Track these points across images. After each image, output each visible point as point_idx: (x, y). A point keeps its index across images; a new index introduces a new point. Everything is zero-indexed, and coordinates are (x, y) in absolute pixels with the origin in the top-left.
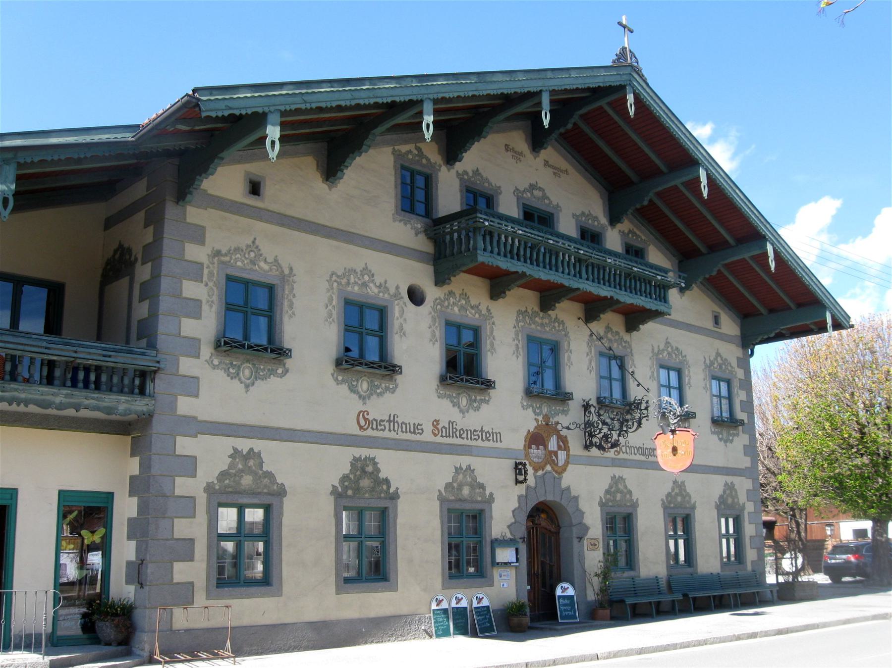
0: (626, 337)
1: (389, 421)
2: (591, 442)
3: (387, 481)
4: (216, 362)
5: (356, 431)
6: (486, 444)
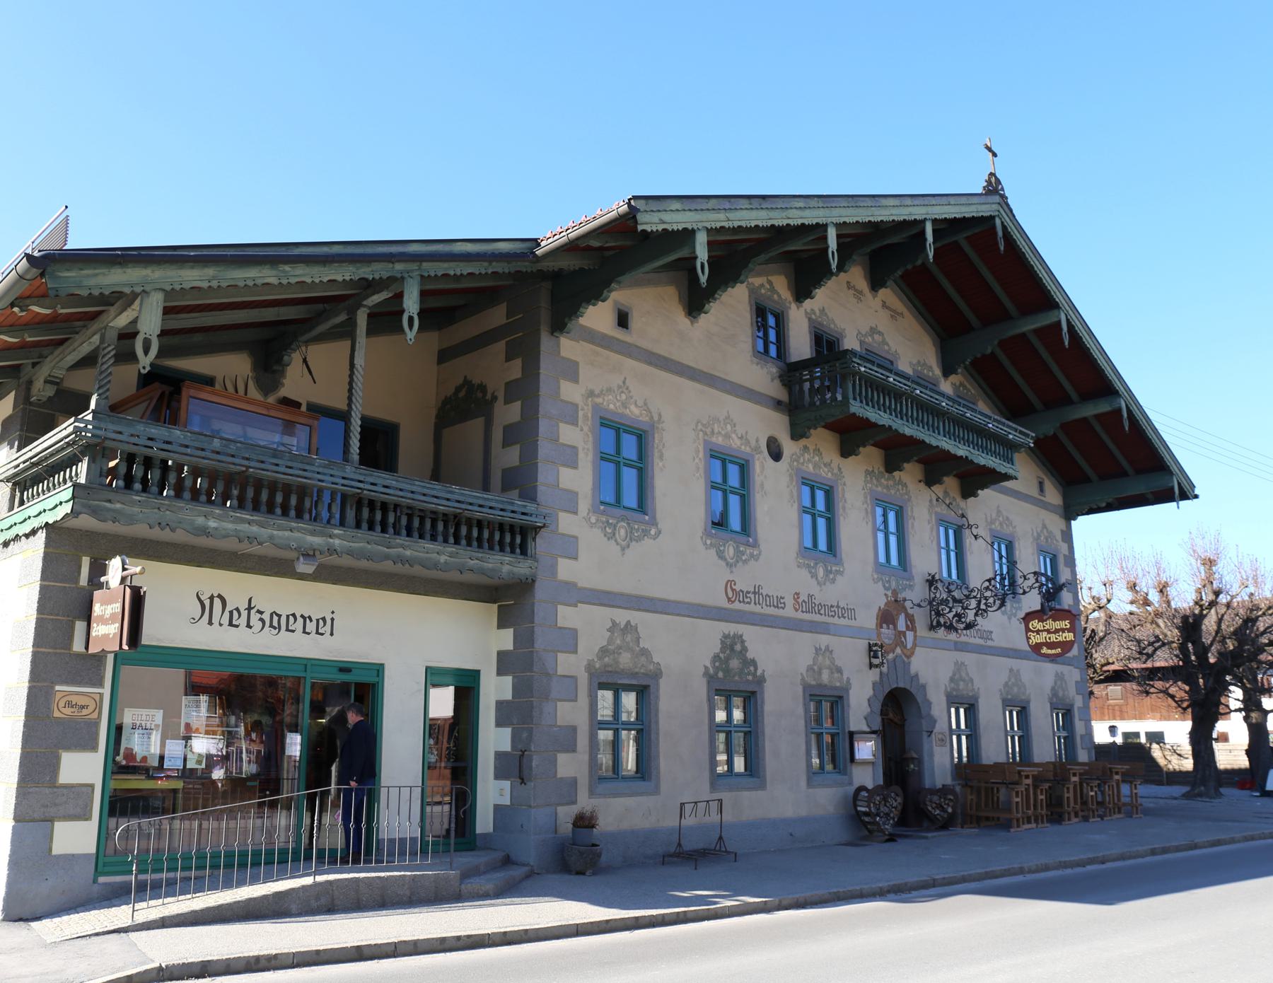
0: (962, 503)
1: (755, 593)
2: (938, 622)
3: (753, 662)
4: (593, 520)
5: (723, 602)
6: (843, 622)
